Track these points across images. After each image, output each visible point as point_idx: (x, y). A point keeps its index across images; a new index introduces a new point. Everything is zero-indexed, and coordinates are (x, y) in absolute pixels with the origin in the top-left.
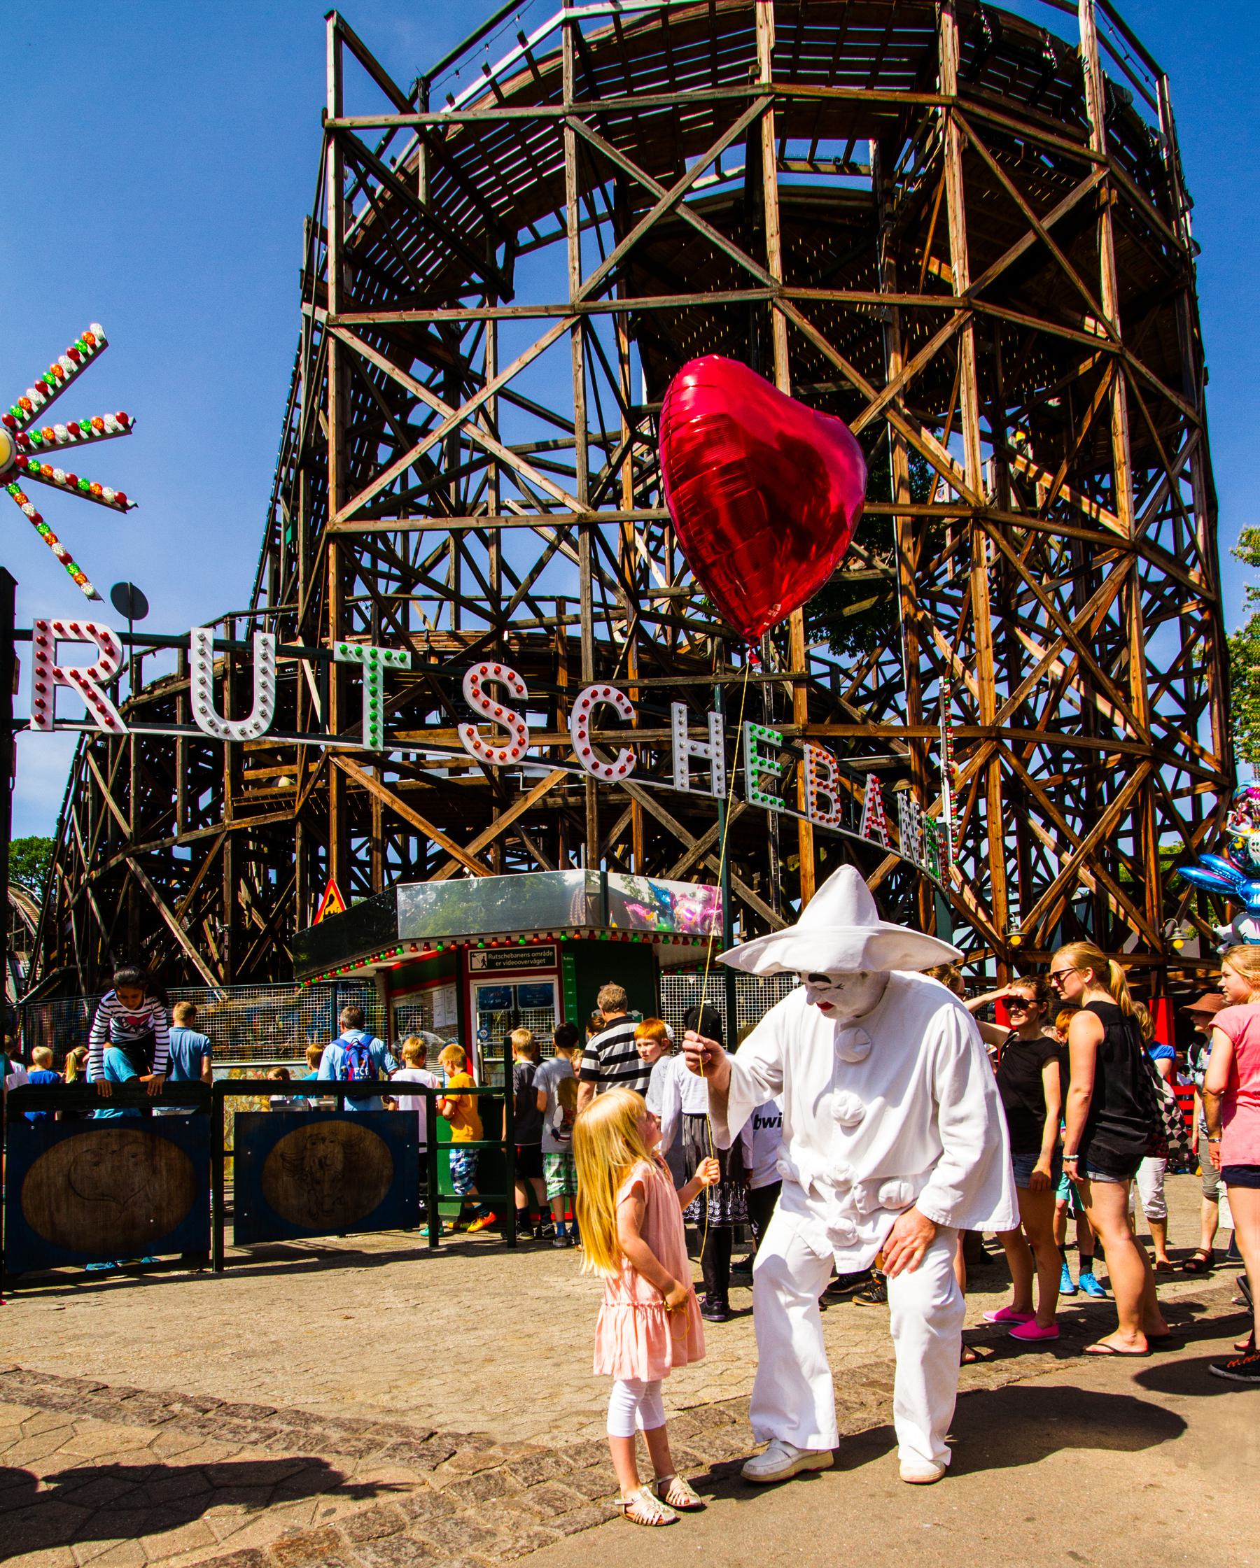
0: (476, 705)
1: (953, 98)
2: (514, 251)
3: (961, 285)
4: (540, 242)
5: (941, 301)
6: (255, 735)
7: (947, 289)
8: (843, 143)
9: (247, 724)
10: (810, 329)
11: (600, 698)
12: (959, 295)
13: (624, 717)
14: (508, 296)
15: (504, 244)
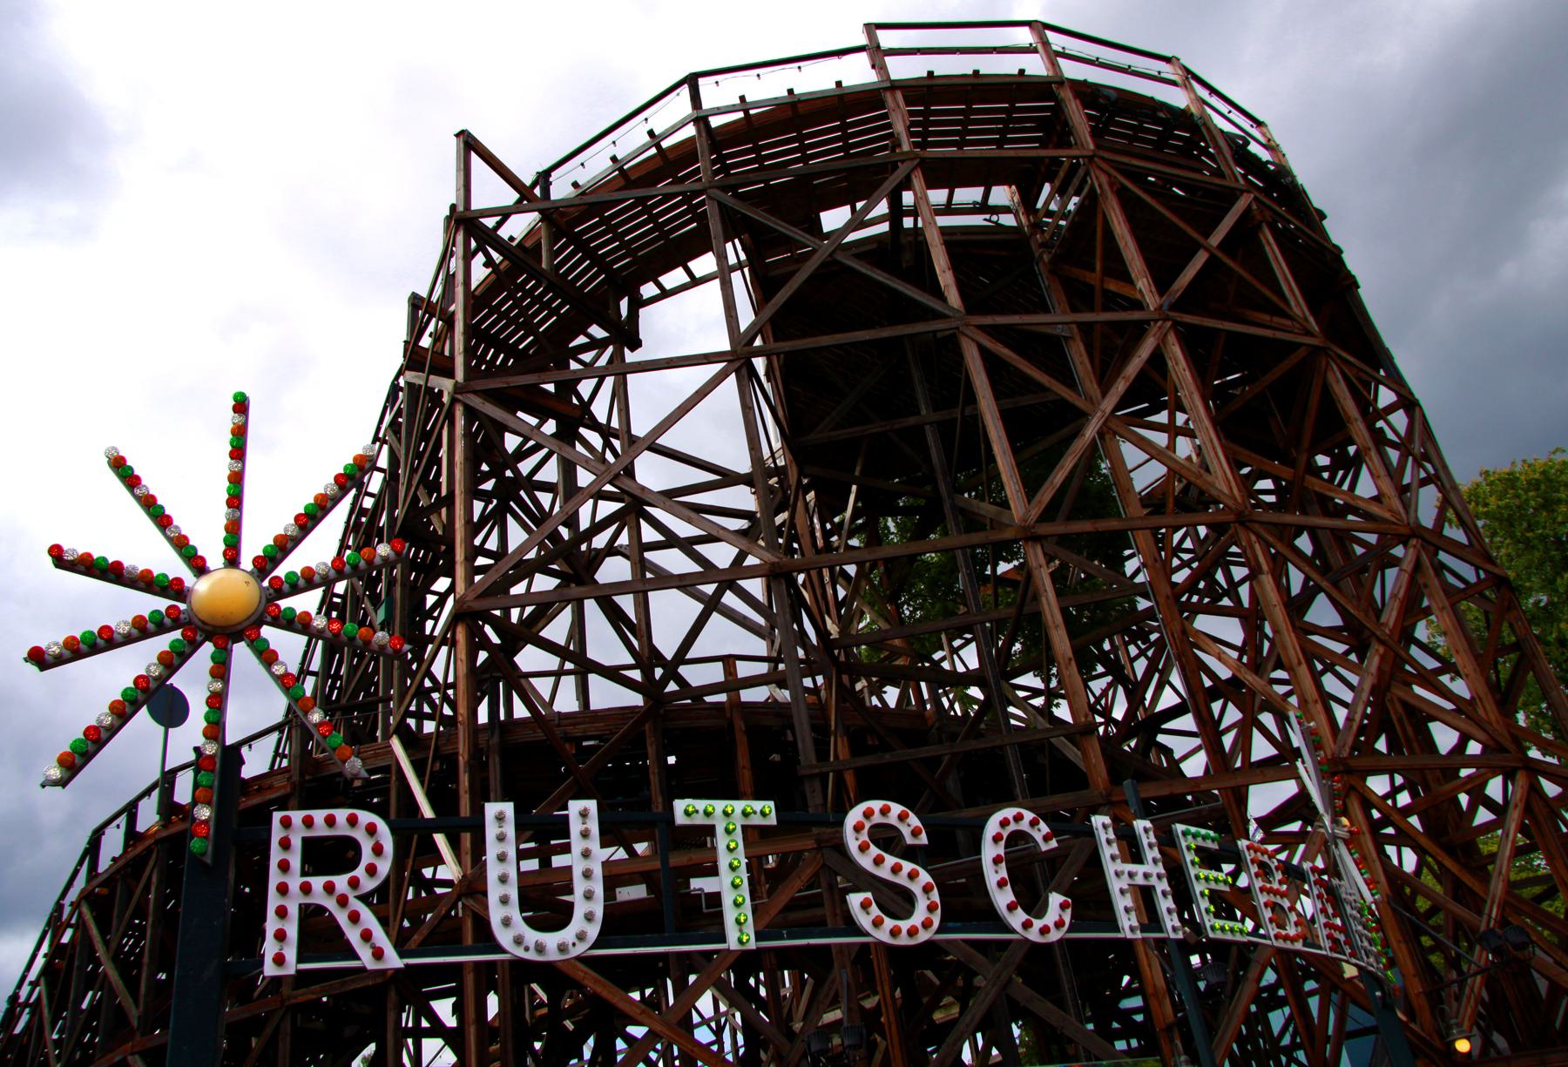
0: (865, 862)
1: (1093, 151)
2: (638, 303)
3: (1151, 300)
4: (665, 294)
5: (1136, 315)
6: (581, 949)
7: (1138, 305)
8: (981, 190)
9: (567, 934)
10: (1005, 352)
11: (877, 818)
12: (1152, 309)
13: (909, 840)
14: (636, 344)
15: (626, 298)
